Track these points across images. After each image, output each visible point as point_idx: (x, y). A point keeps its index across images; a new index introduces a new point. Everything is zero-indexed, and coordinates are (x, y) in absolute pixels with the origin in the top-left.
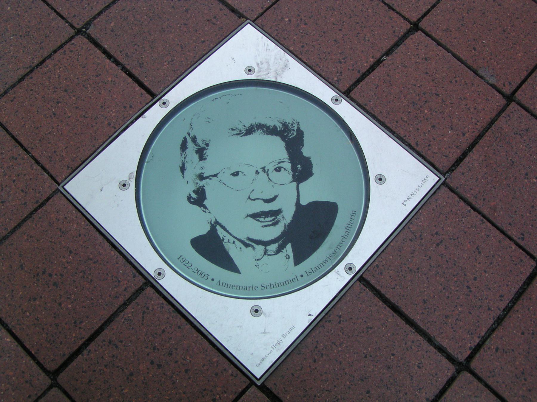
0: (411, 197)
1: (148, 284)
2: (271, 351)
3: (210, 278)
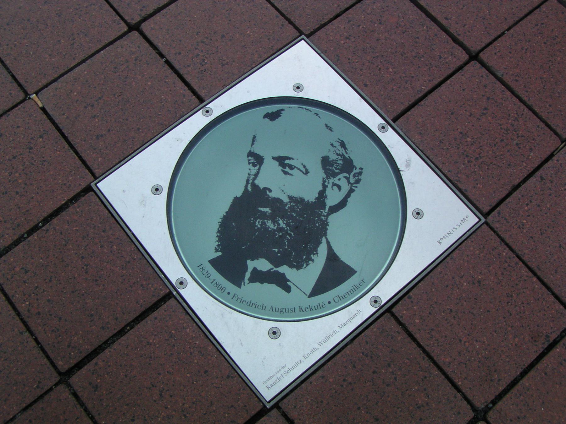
0: (448, 235)
1: (169, 295)
3: (226, 291)
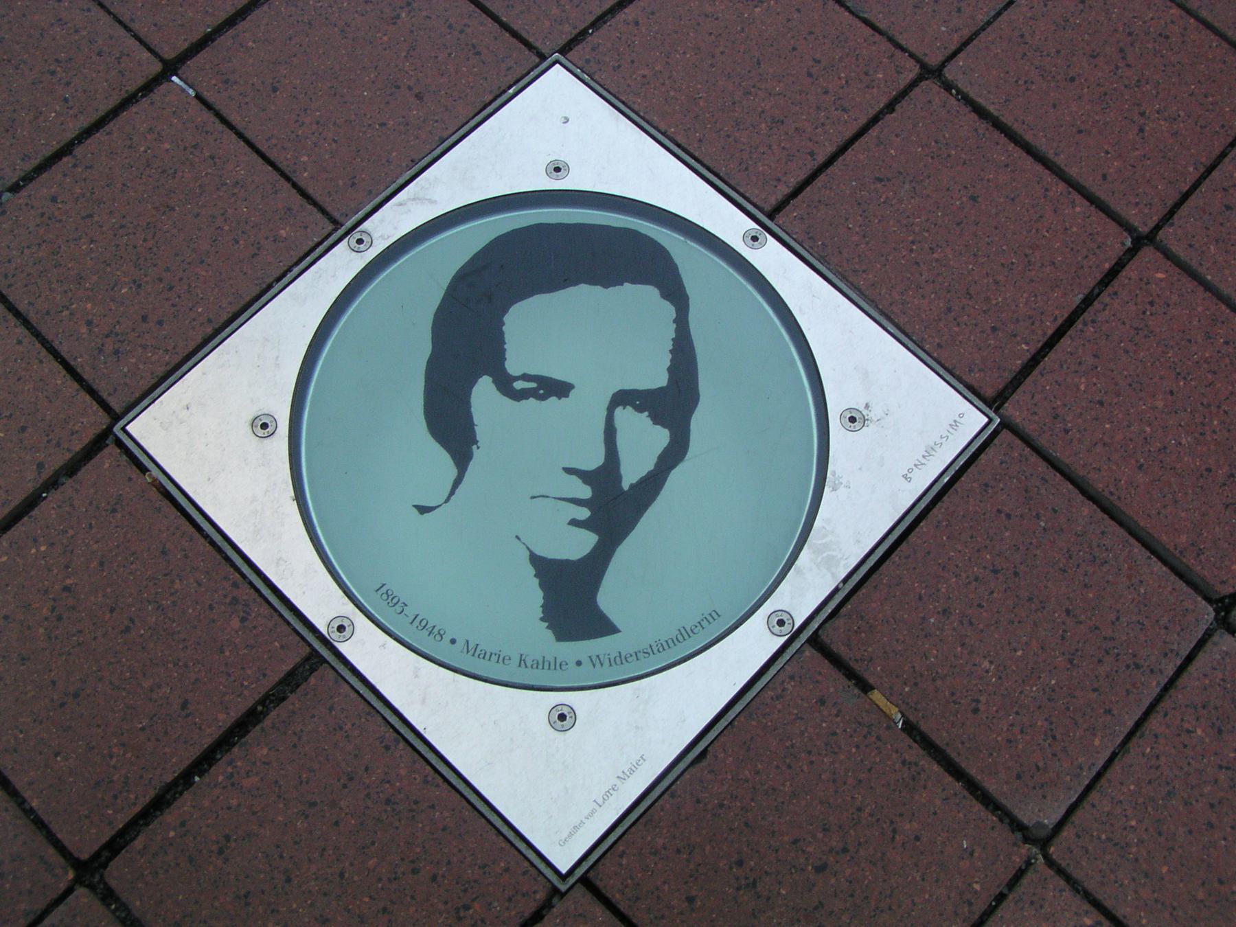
2: (593, 812)
3: (447, 638)
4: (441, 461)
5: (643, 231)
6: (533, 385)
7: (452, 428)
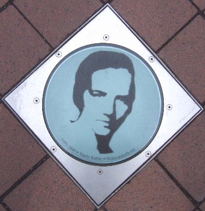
4: (76, 110)
5: (125, 54)
6: (97, 93)
7: (79, 102)
